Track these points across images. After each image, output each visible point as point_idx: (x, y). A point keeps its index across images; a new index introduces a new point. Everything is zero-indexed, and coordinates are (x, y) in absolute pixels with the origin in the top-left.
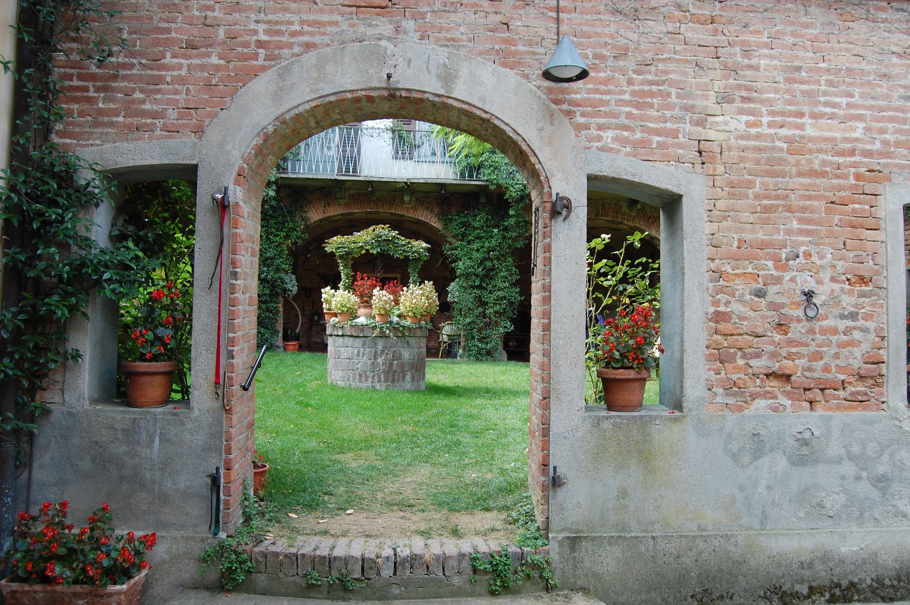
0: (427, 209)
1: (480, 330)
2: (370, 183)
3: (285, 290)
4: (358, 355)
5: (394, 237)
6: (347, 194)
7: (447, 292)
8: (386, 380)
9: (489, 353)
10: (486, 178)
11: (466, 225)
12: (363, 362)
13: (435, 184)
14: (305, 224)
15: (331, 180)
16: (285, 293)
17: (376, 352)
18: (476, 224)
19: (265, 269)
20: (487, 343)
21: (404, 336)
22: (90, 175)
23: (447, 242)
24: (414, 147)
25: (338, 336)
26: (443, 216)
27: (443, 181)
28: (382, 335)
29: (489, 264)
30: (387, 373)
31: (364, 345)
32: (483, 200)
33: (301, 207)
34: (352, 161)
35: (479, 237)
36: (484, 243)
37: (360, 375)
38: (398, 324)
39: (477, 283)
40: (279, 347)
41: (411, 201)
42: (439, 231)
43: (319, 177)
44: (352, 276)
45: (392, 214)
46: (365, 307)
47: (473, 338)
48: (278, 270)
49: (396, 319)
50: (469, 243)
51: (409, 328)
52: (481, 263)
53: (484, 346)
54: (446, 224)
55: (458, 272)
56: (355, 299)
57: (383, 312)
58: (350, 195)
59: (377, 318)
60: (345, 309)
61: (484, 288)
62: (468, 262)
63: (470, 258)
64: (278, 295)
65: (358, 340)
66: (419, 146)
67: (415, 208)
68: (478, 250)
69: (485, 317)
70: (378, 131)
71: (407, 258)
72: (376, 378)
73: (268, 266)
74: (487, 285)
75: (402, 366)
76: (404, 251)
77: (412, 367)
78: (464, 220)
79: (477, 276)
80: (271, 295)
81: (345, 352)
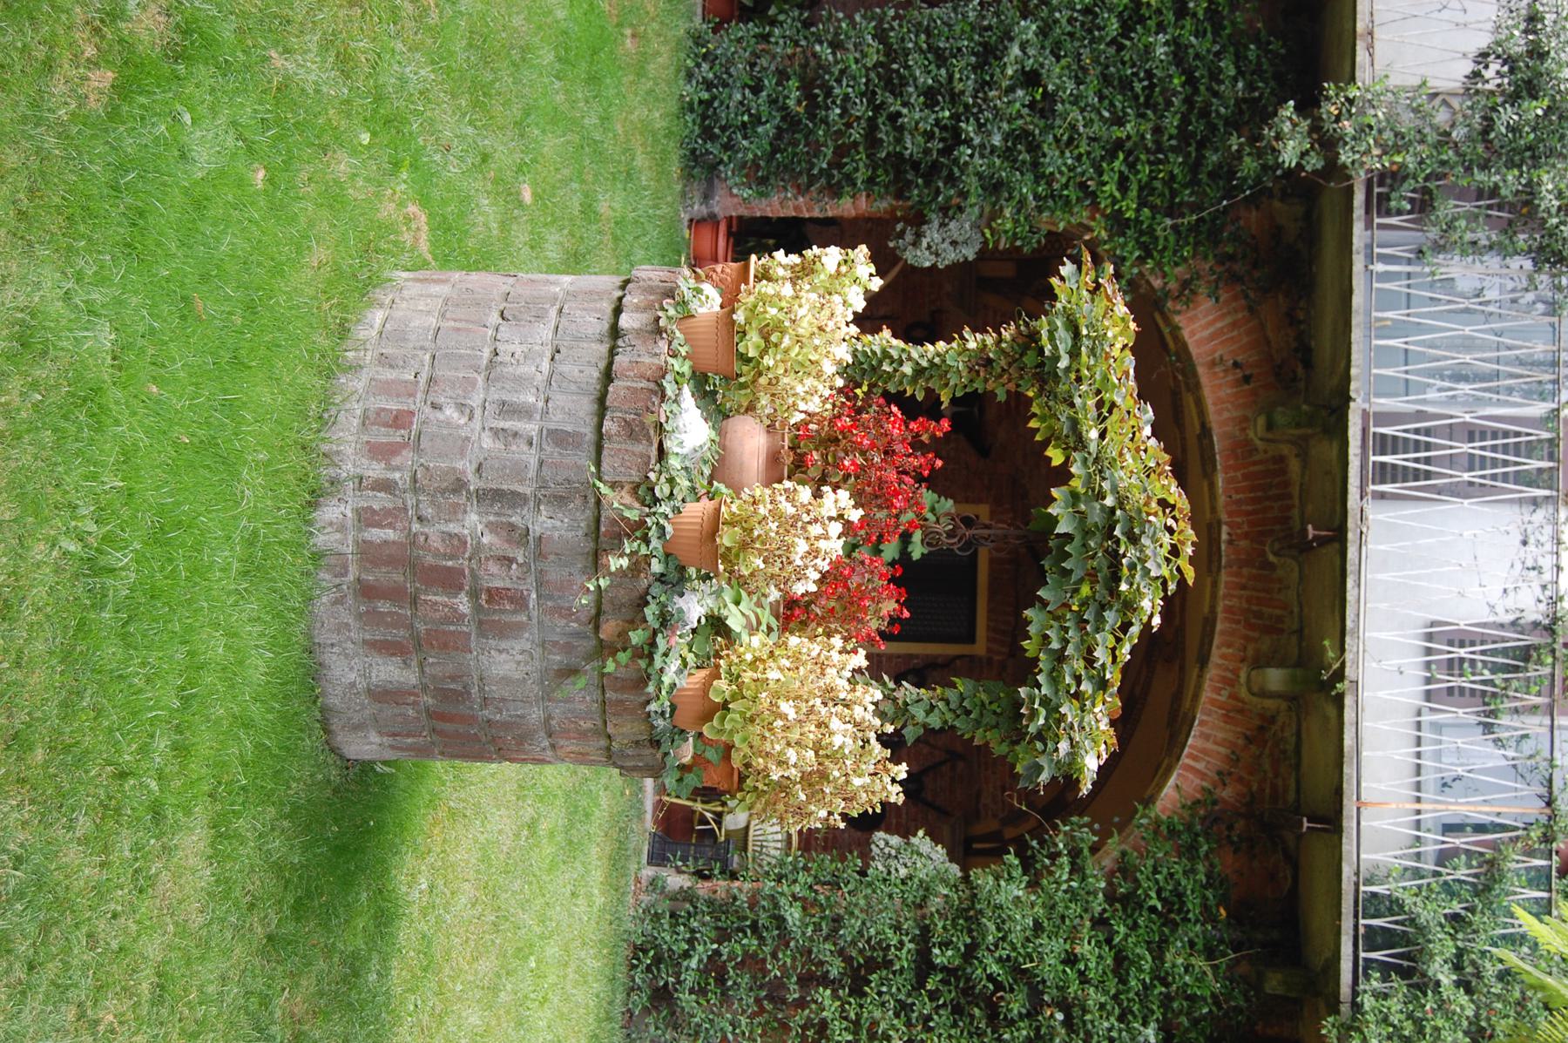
0: (1233, 759)
1: (751, 962)
2: (1338, 535)
3: (918, 220)
4: (507, 410)
5: (1129, 606)
6: (1286, 449)
7: (906, 833)
8: (370, 554)
9: (662, 997)
10: (1368, 1002)
11: (1172, 911)
12: (468, 435)
13: (1339, 792)
14: (1167, 294)
15: (1347, 379)
16: (907, 221)
17: (516, 500)
18: (1175, 958)
19: (997, 140)
20: (700, 991)
21: (605, 649)
22: (1178, 307)
23: (1105, 835)
24: (1487, 704)
25: (618, 311)
26: (1208, 822)
27: (1349, 824)
28: (602, 537)
29: (1016, 1004)
30: (405, 557)
31: (559, 438)
32: (1274, 983)
33: (1234, 278)
34: (1413, 469)
35: (1122, 963)
36: (1100, 985)
37: (399, 420)
38: (665, 620)
39: (939, 957)
40: (707, 197)
41: (1264, 694)
42: (1149, 802)
43: (1356, 335)
44: (932, 397)
45: (1210, 622)
46: (774, 459)
47: (723, 936)
48: (994, 187)
49: (694, 607)
50: (1100, 922)
51: (644, 680)
52: (1018, 972)
53: (690, 979)
54: (1173, 832)
55: (983, 879)
56: (812, 397)
57: (727, 538)
58: (1281, 459)
59: (696, 511)
60: (751, 345)
61: (920, 983)
62: (1021, 922)
63: (1038, 927)
64: (899, 195)
65: (587, 406)
66: (1488, 728)
67: (1234, 711)
68: (1071, 959)
69: (806, 981)
70: (1547, 562)
71: (1025, 671)
72: (380, 501)
73: (1008, 154)
74: (933, 996)
75: (445, 640)
76: (1060, 657)
77: (444, 695)
78: (1193, 904)
79: (970, 953)
80: (898, 162)
81: (526, 349)
